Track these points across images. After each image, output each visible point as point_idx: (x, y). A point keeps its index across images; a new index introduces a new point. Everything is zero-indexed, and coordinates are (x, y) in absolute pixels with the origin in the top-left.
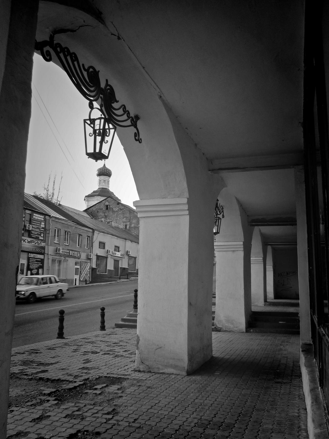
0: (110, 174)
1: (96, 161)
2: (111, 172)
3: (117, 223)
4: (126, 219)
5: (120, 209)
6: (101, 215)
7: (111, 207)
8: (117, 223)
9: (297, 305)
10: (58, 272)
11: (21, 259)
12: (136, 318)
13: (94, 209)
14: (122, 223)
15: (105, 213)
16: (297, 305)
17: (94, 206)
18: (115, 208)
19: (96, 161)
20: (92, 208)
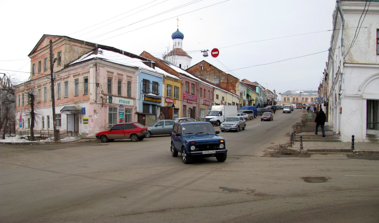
0: (181, 35)
1: (256, 82)
2: (183, 35)
3: (210, 79)
4: (217, 77)
5: (212, 69)
6: (198, 74)
7: (205, 68)
8: (210, 79)
9: (118, 79)
10: (201, 137)
11: (117, 124)
12: (370, 133)
13: (192, 69)
14: (214, 80)
15: (200, 72)
16: (118, 79)
17: (193, 66)
18: (208, 68)
19: (256, 82)
20: (190, 69)
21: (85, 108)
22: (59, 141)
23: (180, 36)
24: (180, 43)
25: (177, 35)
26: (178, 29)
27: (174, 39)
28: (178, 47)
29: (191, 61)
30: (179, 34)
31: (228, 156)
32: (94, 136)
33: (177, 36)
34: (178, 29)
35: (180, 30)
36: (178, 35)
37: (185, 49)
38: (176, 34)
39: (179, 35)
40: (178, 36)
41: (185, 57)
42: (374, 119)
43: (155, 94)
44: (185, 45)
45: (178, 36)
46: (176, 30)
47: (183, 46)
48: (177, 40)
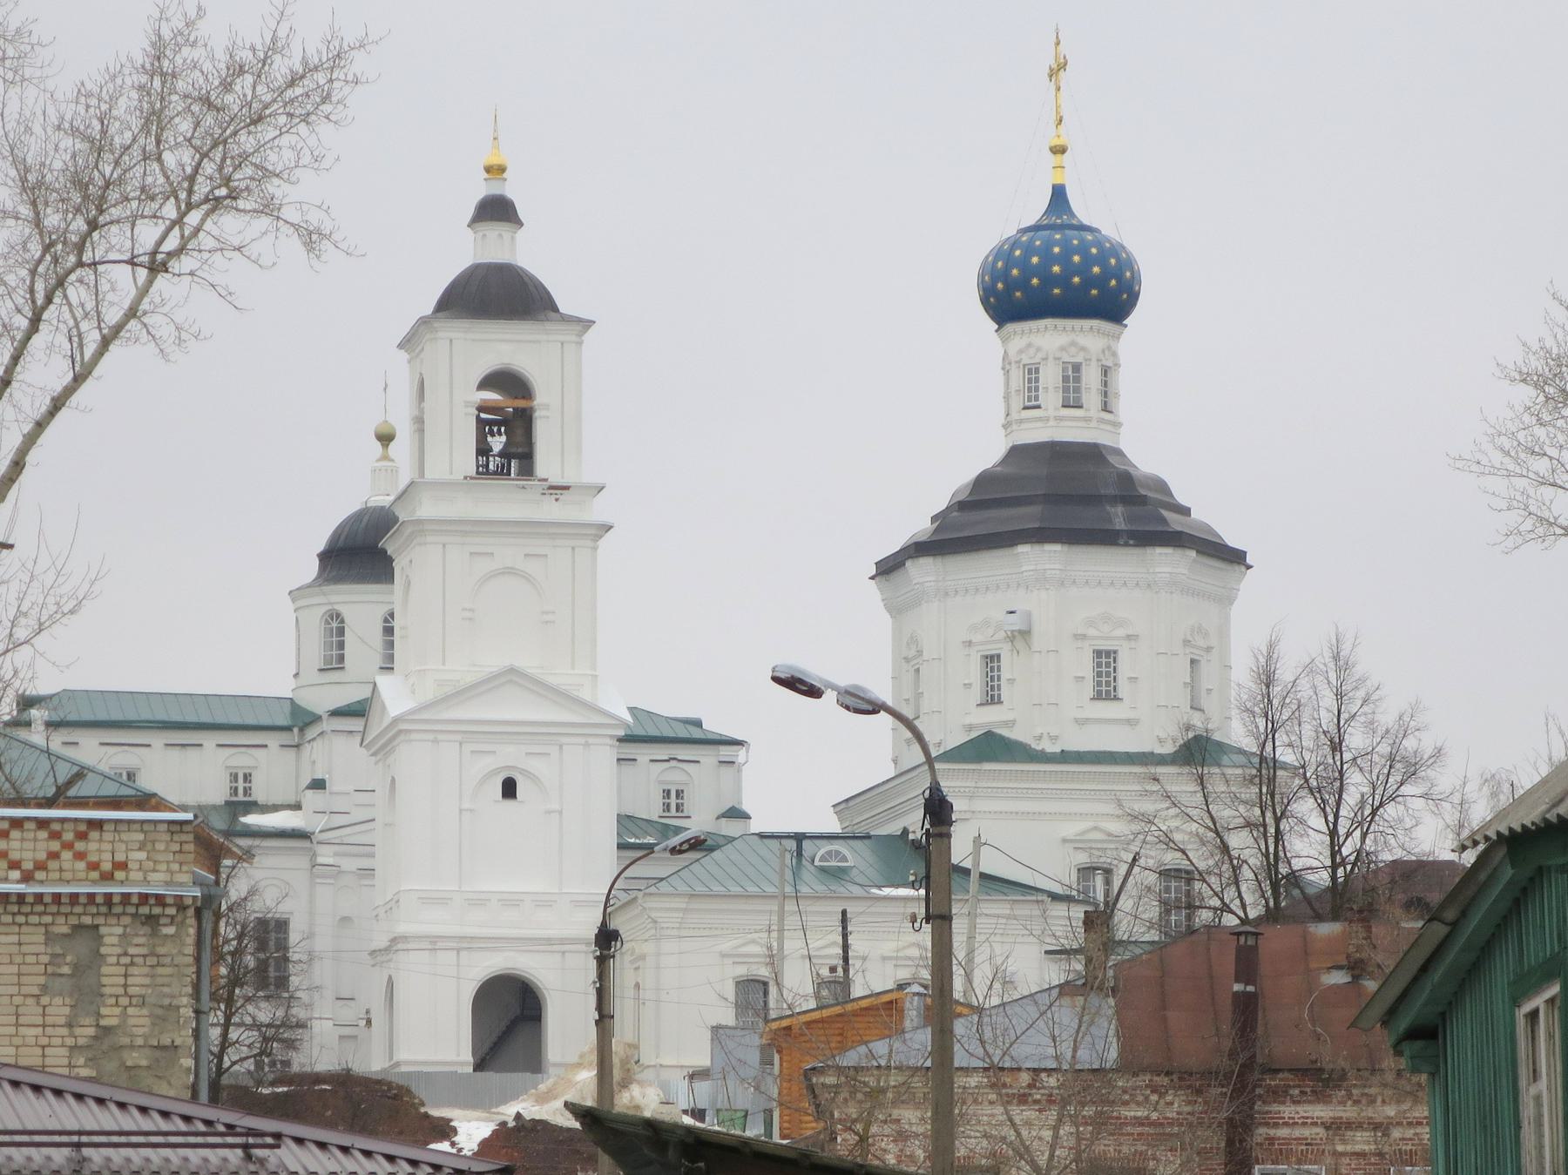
0: (1101, 259)
2: (1129, 263)
21: (738, 983)
22: (206, 890)
23: (1101, 282)
24: (1091, 377)
25: (1048, 259)
26: (1059, 196)
27: (1010, 327)
28: (1055, 425)
29: (1230, 600)
30: (1068, 251)
31: (555, 1065)
32: (462, 1064)
33: (1023, 283)
34: (1059, 196)
35: (1084, 209)
36: (1064, 259)
37: (1146, 445)
38: (1029, 250)
39: (1089, 281)
40: (1059, 283)
41: (1166, 562)
42: (87, 716)
43: (904, 885)
44: (1158, 404)
45: (1059, 283)
46: (1034, 209)
47: (1125, 406)
48: (1050, 338)
